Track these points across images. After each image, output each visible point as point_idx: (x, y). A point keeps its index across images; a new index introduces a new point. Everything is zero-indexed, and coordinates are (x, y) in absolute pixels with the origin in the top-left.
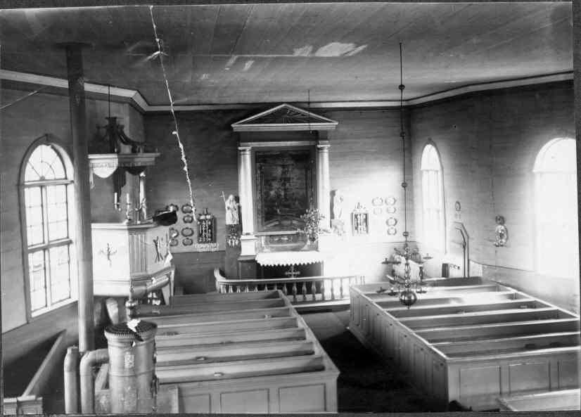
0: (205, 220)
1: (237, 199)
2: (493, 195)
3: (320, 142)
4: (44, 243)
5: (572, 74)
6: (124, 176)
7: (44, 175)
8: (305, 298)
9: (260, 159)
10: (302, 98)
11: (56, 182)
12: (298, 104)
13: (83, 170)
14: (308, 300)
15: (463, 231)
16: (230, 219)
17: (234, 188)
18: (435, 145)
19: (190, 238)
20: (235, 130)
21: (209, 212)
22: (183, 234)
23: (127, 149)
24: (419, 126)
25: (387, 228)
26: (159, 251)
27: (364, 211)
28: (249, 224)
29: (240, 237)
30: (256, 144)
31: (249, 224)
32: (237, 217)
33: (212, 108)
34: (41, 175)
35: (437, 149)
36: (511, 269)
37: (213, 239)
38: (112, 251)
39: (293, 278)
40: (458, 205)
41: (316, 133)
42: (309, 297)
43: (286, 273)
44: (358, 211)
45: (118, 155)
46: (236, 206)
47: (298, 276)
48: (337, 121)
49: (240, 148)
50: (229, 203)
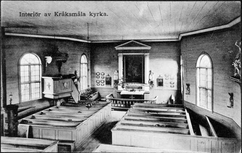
0: (108, 78)
1: (118, 71)
3: (119, 54)
7: (30, 62)
8: (121, 105)
9: (126, 58)
13: (44, 61)
17: (117, 66)
22: (101, 82)
25: (170, 85)
33: (118, 41)
38: (50, 85)
39: (132, 99)
43: (130, 97)
44: (159, 78)
47: (134, 99)
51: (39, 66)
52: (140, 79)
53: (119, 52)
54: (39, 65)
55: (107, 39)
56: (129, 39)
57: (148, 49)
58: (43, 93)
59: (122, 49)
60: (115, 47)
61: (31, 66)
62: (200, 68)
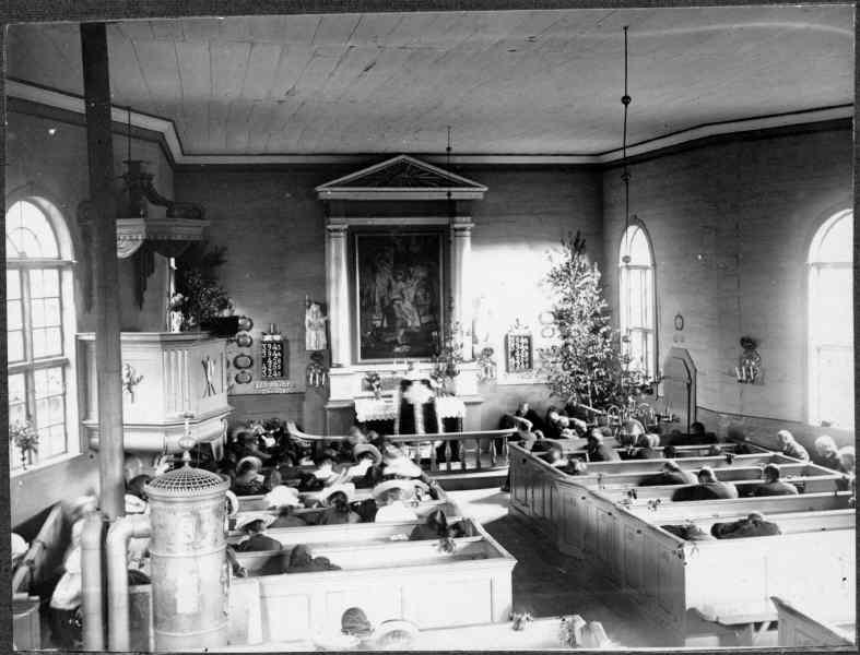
0: (273, 343)
2: (739, 303)
4: (25, 360)
5: (852, 108)
6: (151, 260)
8: (449, 467)
10: (435, 144)
11: (45, 265)
12: (424, 157)
14: (468, 467)
15: (687, 361)
16: (313, 340)
17: (321, 283)
18: (643, 225)
19: (247, 371)
20: (322, 196)
21: (278, 329)
23: (158, 211)
24: (616, 195)
26: (209, 378)
27: (526, 333)
28: (343, 349)
29: (328, 371)
30: (355, 221)
31: (343, 349)
32: (323, 341)
34: (20, 250)
35: (647, 233)
36: (786, 421)
37: (283, 373)
40: (679, 320)
41: (452, 203)
42: (456, 466)
44: (516, 332)
45: (146, 221)
46: (322, 321)
48: (487, 186)
49: (329, 227)
50: (311, 315)
51: (55, 273)
52: (430, 343)
53: (329, 209)
54: (60, 268)
55: (293, 144)
56: (390, 151)
57: (473, 196)
58: (406, 395)
59: (351, 197)
60: (319, 189)
61: (33, 273)
62: (819, 268)
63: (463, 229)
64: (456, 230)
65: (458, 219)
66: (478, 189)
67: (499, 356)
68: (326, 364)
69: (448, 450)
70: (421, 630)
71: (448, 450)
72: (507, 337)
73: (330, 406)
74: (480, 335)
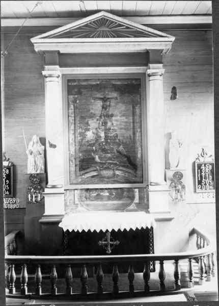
63: (154, 75)
64: (149, 76)
65: (151, 65)
66: (166, 39)
67: (188, 180)
68: (44, 184)
69: (101, 34)
70: (177, 167)
71: (101, 34)
72: (194, 163)
73: (44, 220)
74: (173, 163)
